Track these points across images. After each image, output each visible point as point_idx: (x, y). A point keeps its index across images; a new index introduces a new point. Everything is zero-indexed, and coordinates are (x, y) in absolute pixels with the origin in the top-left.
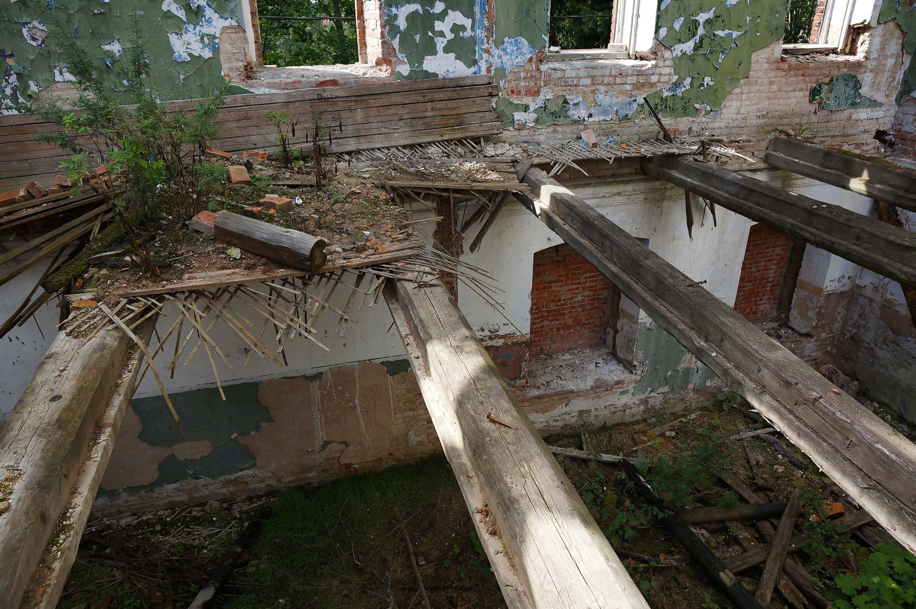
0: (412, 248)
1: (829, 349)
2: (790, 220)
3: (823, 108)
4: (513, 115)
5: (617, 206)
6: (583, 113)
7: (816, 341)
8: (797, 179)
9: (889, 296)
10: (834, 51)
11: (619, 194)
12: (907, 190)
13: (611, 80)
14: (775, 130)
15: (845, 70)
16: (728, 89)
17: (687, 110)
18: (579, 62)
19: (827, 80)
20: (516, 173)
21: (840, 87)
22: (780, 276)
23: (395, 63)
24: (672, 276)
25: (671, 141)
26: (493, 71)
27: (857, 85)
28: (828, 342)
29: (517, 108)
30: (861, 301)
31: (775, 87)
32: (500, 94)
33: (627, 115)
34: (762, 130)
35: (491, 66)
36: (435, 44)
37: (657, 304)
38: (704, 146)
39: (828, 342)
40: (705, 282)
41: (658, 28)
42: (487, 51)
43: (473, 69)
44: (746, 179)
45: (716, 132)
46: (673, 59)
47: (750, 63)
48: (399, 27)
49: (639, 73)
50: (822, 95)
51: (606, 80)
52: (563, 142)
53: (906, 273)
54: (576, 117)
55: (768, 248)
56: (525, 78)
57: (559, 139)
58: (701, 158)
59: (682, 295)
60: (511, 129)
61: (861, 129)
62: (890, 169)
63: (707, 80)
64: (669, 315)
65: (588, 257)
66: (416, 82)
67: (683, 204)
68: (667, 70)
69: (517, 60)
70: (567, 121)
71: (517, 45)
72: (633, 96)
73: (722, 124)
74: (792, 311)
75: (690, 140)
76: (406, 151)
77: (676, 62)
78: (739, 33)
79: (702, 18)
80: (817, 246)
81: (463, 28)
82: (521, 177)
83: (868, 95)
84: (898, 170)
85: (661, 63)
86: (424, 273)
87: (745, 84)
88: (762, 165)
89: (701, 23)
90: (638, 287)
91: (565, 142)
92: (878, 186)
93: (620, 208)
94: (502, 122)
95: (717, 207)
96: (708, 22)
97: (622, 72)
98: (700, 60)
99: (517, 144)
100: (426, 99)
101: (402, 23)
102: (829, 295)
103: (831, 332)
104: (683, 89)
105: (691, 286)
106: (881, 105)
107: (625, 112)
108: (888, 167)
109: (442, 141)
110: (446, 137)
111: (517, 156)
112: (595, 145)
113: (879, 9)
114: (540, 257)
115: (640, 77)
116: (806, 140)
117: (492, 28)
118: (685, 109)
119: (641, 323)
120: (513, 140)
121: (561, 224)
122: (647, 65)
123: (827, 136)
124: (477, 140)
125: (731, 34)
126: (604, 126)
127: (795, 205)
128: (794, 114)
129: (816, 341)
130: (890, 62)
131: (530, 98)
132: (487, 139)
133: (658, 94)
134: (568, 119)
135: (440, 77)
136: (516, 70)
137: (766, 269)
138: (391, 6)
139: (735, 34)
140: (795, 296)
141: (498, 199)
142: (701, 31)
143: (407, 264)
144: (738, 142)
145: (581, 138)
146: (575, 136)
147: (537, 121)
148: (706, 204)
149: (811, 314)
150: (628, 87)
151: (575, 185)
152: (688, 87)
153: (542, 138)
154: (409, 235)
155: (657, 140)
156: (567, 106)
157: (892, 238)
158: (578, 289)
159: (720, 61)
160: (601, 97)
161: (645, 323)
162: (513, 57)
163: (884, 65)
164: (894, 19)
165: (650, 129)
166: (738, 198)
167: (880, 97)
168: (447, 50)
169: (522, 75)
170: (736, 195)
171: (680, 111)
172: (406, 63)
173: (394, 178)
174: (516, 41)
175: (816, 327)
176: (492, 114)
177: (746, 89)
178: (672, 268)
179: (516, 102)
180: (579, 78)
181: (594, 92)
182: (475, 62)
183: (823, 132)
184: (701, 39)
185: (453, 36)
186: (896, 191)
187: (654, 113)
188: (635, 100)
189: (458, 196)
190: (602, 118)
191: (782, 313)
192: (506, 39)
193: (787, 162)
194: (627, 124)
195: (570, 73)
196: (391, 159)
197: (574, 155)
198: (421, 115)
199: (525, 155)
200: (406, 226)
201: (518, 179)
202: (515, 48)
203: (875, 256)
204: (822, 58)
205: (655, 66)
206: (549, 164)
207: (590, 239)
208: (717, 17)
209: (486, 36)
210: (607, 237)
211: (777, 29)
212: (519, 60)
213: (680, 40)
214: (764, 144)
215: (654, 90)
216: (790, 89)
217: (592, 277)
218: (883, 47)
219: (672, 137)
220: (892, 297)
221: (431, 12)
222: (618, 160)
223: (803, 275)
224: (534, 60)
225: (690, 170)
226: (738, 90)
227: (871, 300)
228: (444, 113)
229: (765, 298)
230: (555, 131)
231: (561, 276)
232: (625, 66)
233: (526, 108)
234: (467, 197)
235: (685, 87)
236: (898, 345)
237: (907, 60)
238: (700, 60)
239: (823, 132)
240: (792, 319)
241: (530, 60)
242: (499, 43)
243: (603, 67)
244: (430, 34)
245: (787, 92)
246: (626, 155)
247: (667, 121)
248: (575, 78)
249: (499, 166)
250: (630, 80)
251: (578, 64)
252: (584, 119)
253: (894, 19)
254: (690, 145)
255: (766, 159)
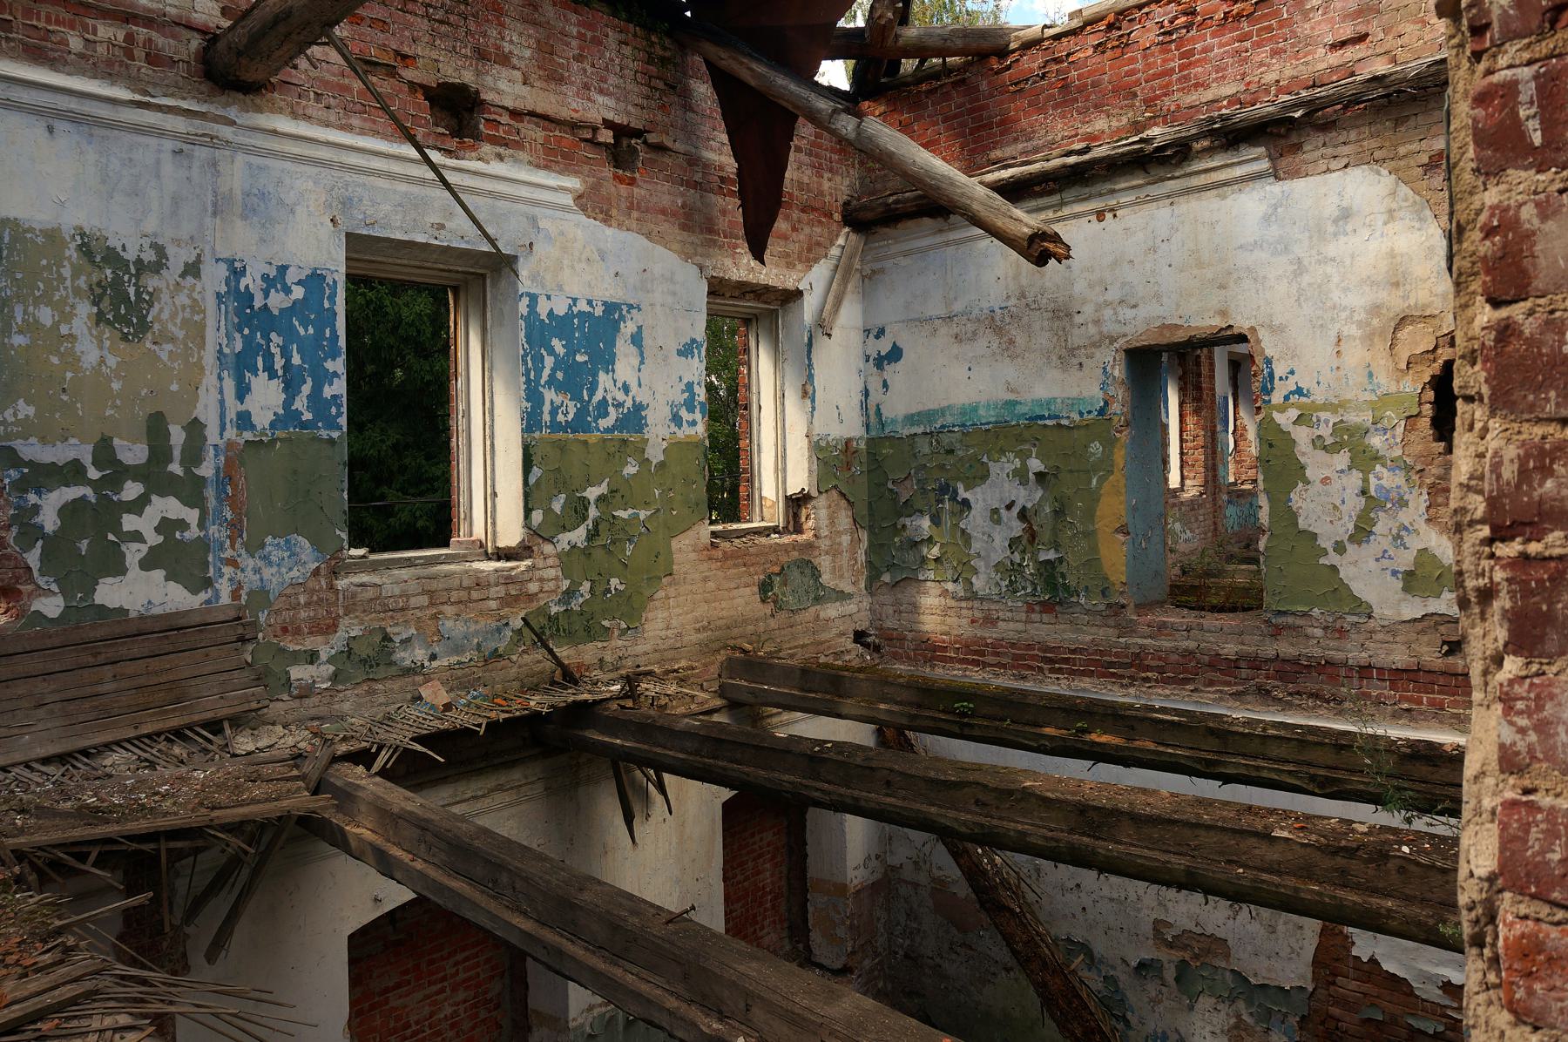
0: (76, 980)
1: (881, 985)
2: (786, 777)
3: (781, 609)
4: (287, 673)
5: (499, 810)
6: (420, 654)
7: (859, 976)
8: (771, 716)
9: (937, 873)
10: (775, 530)
11: (499, 788)
12: (919, 706)
13: (463, 594)
14: (725, 647)
15: (795, 554)
16: (647, 593)
17: (592, 631)
18: (403, 571)
19: (777, 569)
20: (302, 778)
21: (795, 574)
22: (780, 878)
23: (30, 595)
24: (634, 913)
25: (576, 683)
26: (244, 597)
27: (816, 573)
28: (876, 973)
29: (295, 658)
30: (903, 890)
31: (711, 585)
32: (260, 635)
33: (496, 650)
34: (706, 649)
35: (240, 587)
36: (123, 555)
37: (618, 972)
38: (631, 681)
39: (876, 973)
40: (693, 908)
41: (528, 512)
42: (232, 562)
43: (203, 596)
44: (705, 725)
45: (641, 661)
46: (558, 556)
47: (670, 553)
48: (42, 527)
49: (509, 580)
50: (776, 590)
51: (455, 596)
52: (388, 709)
53: (965, 823)
54: (407, 663)
55: (753, 835)
56: (308, 604)
57: (380, 705)
58: (629, 703)
59: (660, 942)
60: (285, 697)
61: (834, 631)
62: (890, 679)
63: (614, 582)
64: (644, 988)
65: (469, 915)
66: (78, 628)
67: (612, 787)
68: (552, 573)
69: (292, 574)
70: (393, 670)
71: (289, 549)
72: (502, 617)
73: (648, 647)
74: (959, 873)
75: (606, 677)
76: (50, 769)
77: (564, 559)
78: (649, 513)
79: (592, 493)
80: (837, 810)
81: (182, 524)
82: (312, 785)
83: (832, 584)
84: (901, 680)
85: (540, 563)
86: (115, 1030)
87: (670, 584)
88: (718, 702)
89: (592, 502)
90: (576, 950)
91: (392, 709)
92: (882, 706)
93: (506, 813)
94: (266, 686)
95: (668, 778)
96: (601, 499)
97: (480, 583)
98: (598, 554)
99: (300, 723)
100: (101, 659)
101: (49, 520)
102: (858, 892)
103: (876, 954)
104: (581, 600)
105: (670, 921)
106: (850, 596)
107: (492, 645)
108: (887, 677)
109: (138, 738)
110: (147, 729)
111: (302, 745)
112: (448, 707)
113: (815, 474)
114: (361, 942)
115: (511, 587)
116: (770, 655)
117: (241, 521)
118: (588, 630)
119: (575, 1029)
120: (290, 718)
121: (407, 860)
122: (518, 567)
123: (796, 647)
124: (215, 726)
125: (638, 515)
126: (460, 673)
127: (789, 752)
128: (745, 622)
129: (859, 976)
130: (846, 539)
131: (320, 639)
132: (237, 722)
133: (543, 611)
134: (394, 668)
135: (133, 615)
136: (289, 591)
137: (758, 873)
138: (26, 491)
139: (643, 515)
140: (810, 909)
141: (266, 839)
142: (593, 512)
143: (68, 1019)
144: (676, 671)
145: (420, 698)
146: (409, 696)
147: (335, 677)
148: (648, 780)
149: (841, 932)
150: (493, 604)
151: (419, 785)
152: (588, 596)
153: (347, 706)
154: (67, 950)
155: (553, 683)
156: (390, 645)
157: (932, 774)
158: (442, 991)
159: (628, 553)
160: (449, 624)
161: (582, 1025)
162: (284, 570)
163: (840, 544)
164: (835, 487)
165: (539, 667)
166: (702, 756)
167: (848, 589)
168: (146, 564)
169: (302, 600)
170: (697, 753)
171: (582, 633)
172: (54, 594)
173: (21, 831)
174: (287, 541)
175: (853, 953)
176: (246, 673)
177: (672, 591)
178: (631, 897)
179: (292, 647)
180: (408, 597)
181: (435, 617)
182: (208, 583)
183: (789, 641)
184: (596, 523)
185: (161, 539)
186: (907, 709)
187: (541, 640)
188: (507, 624)
189: (179, 844)
190: (453, 659)
191: (798, 942)
192: (269, 539)
193: (753, 692)
194: (499, 665)
195: (390, 589)
196: (12, 792)
197: (414, 729)
198: (88, 690)
199: (317, 741)
200: (59, 932)
201: (307, 789)
202: (286, 554)
203: (917, 806)
204: (763, 540)
205: (533, 568)
206: (366, 751)
207: (470, 879)
208: (613, 491)
209: (228, 537)
210: (501, 867)
211: (697, 505)
212: (295, 573)
213: (564, 527)
214: (714, 670)
215: (535, 605)
216: (733, 585)
217: (467, 959)
218: (832, 521)
219: (577, 676)
220: (941, 873)
221: (115, 498)
222: (493, 726)
223: (812, 872)
224: (323, 572)
225: (616, 725)
226: (661, 594)
227: (916, 885)
228: (142, 681)
229: (766, 923)
230: (371, 692)
231: (406, 972)
232: (483, 571)
233: (312, 657)
234: (200, 843)
235: (582, 596)
236: (971, 948)
237: (864, 536)
238: (598, 554)
239: (789, 641)
240: (816, 951)
241: (316, 572)
242: (255, 547)
243: (447, 575)
244: (111, 537)
245: (729, 590)
246: (507, 715)
247: (563, 652)
248: (401, 596)
249: (266, 770)
250: (494, 592)
251: (404, 573)
252: (423, 665)
253: (835, 487)
254: (608, 684)
255: (722, 692)
